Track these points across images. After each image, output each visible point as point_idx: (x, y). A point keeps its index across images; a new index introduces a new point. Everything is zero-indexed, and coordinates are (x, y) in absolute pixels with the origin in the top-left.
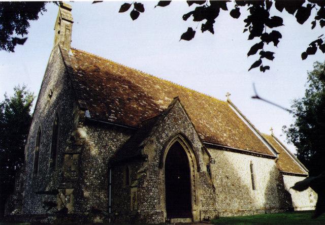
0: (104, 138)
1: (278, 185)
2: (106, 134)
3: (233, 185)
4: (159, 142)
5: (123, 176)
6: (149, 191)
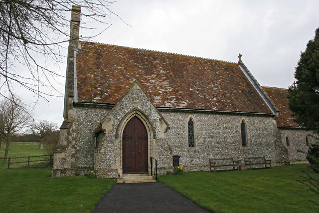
0: (90, 115)
1: (275, 141)
2: (92, 112)
3: (218, 143)
4: (117, 119)
5: (249, 128)
6: (105, 155)
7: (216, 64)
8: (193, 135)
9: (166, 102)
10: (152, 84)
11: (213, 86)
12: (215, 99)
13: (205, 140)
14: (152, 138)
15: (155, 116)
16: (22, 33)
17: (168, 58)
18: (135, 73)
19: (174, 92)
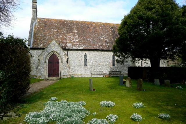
3: (99, 65)
6: (40, 70)
7: (107, 25)
8: (87, 61)
9: (73, 46)
10: (69, 38)
11: (101, 37)
12: (100, 44)
13: (92, 63)
17: (81, 24)
18: (61, 33)
19: (79, 42)
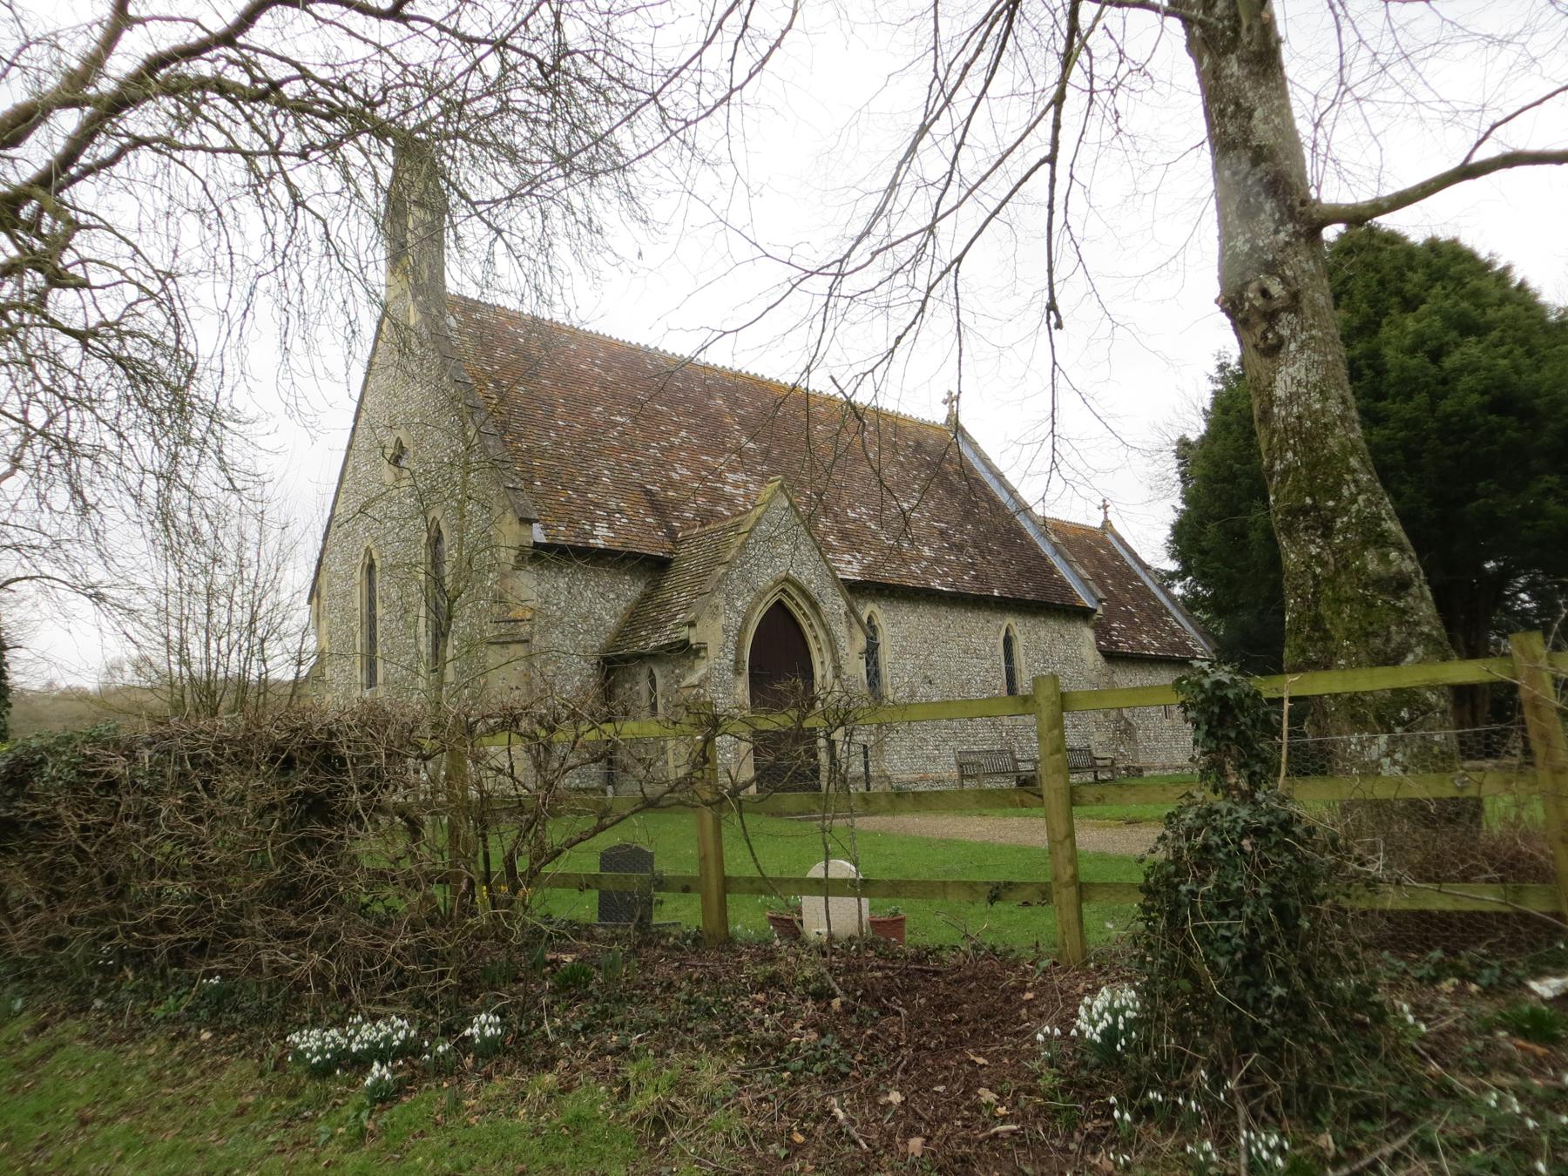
14: (829, 676)
15: (834, 604)
16: (518, 27)
